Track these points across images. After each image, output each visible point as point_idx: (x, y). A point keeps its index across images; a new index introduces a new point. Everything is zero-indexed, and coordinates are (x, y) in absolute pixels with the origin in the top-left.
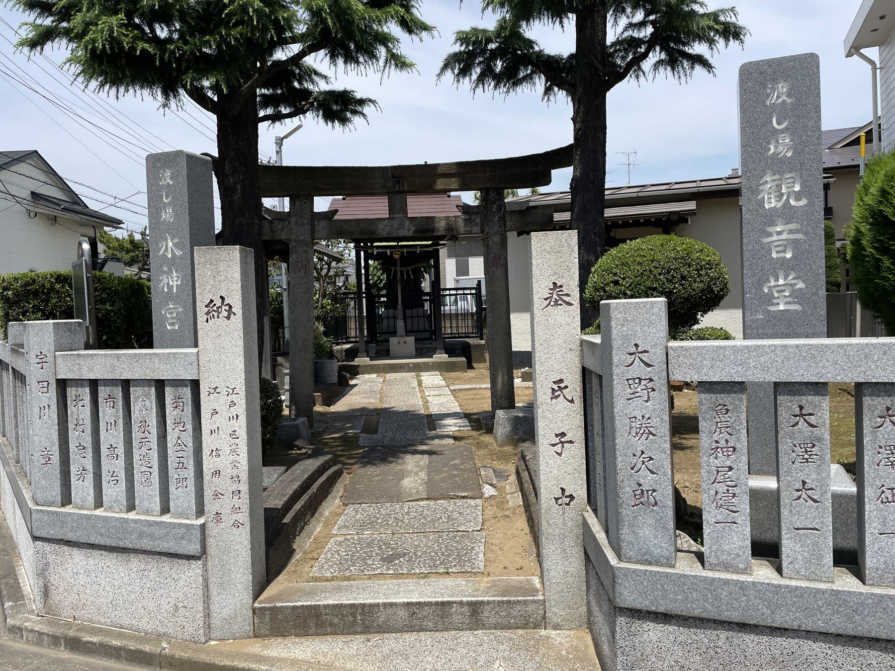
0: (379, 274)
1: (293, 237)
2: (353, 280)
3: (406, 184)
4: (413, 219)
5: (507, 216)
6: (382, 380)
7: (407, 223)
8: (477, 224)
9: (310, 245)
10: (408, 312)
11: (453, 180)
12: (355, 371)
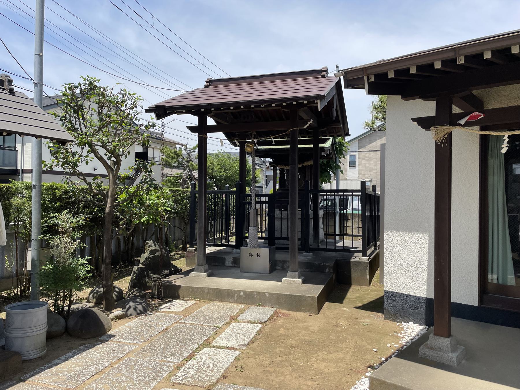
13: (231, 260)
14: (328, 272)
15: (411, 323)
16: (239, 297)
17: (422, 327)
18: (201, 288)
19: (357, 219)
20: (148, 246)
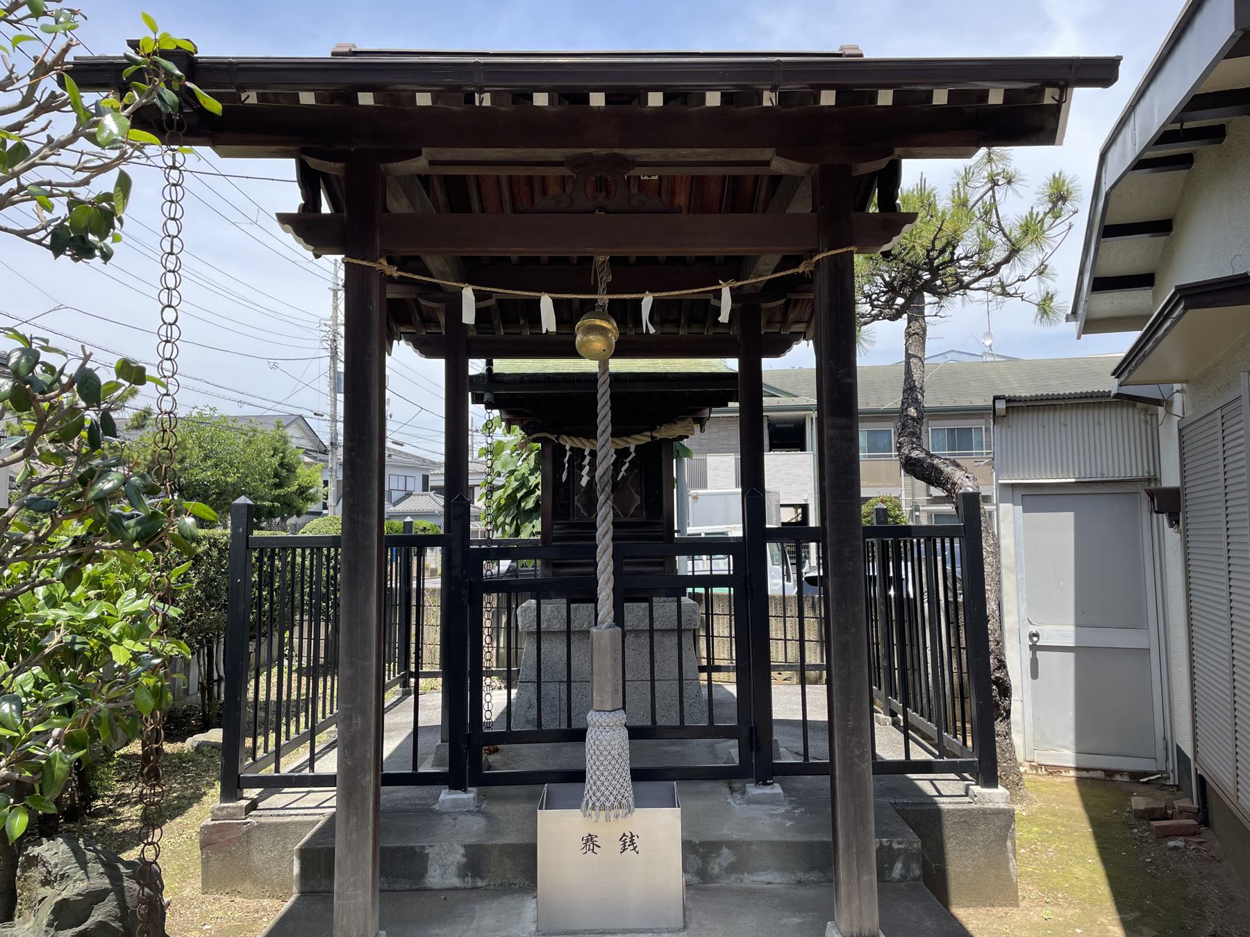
10: (635, 612)
14: (903, 878)
19: (780, 613)
20: (37, 873)
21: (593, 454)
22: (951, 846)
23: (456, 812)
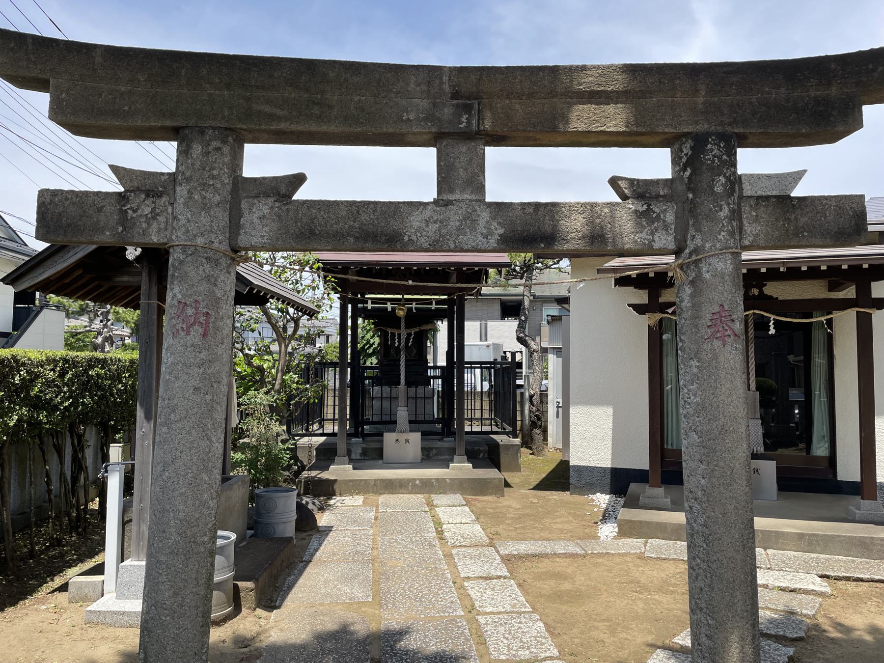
0: (368, 336)
1: (178, 238)
2: (335, 339)
3: (488, 114)
4: (500, 207)
5: (746, 208)
6: (372, 515)
7: (485, 216)
8: (666, 227)
9: (224, 262)
10: (412, 390)
11: (610, 109)
12: (325, 490)
13: (360, 451)
15: (598, 494)
16: (414, 486)
17: (608, 496)
18: (366, 481)
21: (399, 335)
22: (502, 455)
23: (357, 443)
